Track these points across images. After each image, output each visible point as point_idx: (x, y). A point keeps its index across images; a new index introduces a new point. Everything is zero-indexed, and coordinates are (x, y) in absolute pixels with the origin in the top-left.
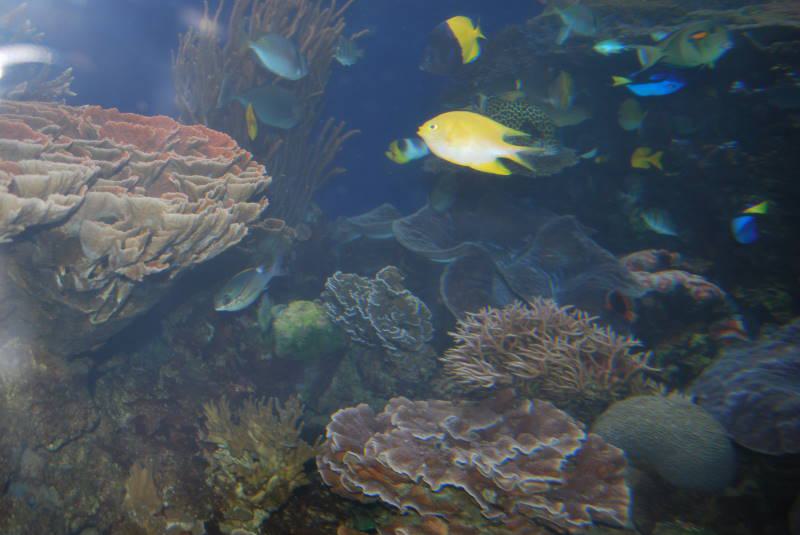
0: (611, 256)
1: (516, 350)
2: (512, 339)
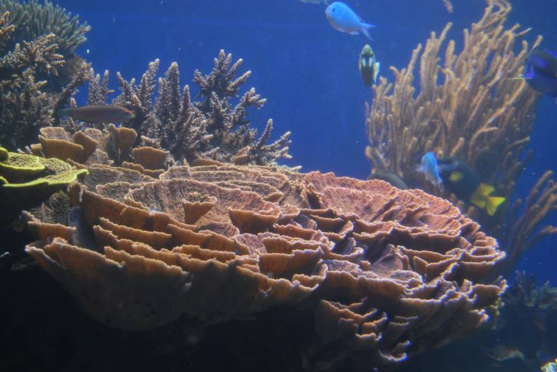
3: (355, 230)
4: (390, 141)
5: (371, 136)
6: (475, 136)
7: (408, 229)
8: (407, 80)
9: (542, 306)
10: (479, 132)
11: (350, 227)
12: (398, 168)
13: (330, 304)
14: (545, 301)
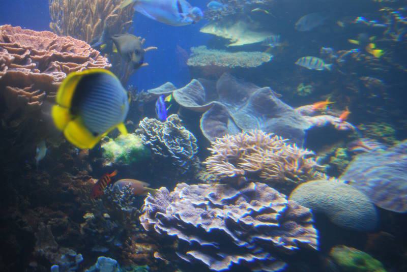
0: (290, 108)
1: (244, 157)
2: (242, 151)
3: (31, 54)
4: (63, 19)
5: (53, 16)
6: (107, 18)
7: (62, 54)
8: (358, 173)
9: (141, 101)
10: (109, 16)
11: (28, 52)
12: (67, 32)
13: (15, 90)
14: (142, 98)
